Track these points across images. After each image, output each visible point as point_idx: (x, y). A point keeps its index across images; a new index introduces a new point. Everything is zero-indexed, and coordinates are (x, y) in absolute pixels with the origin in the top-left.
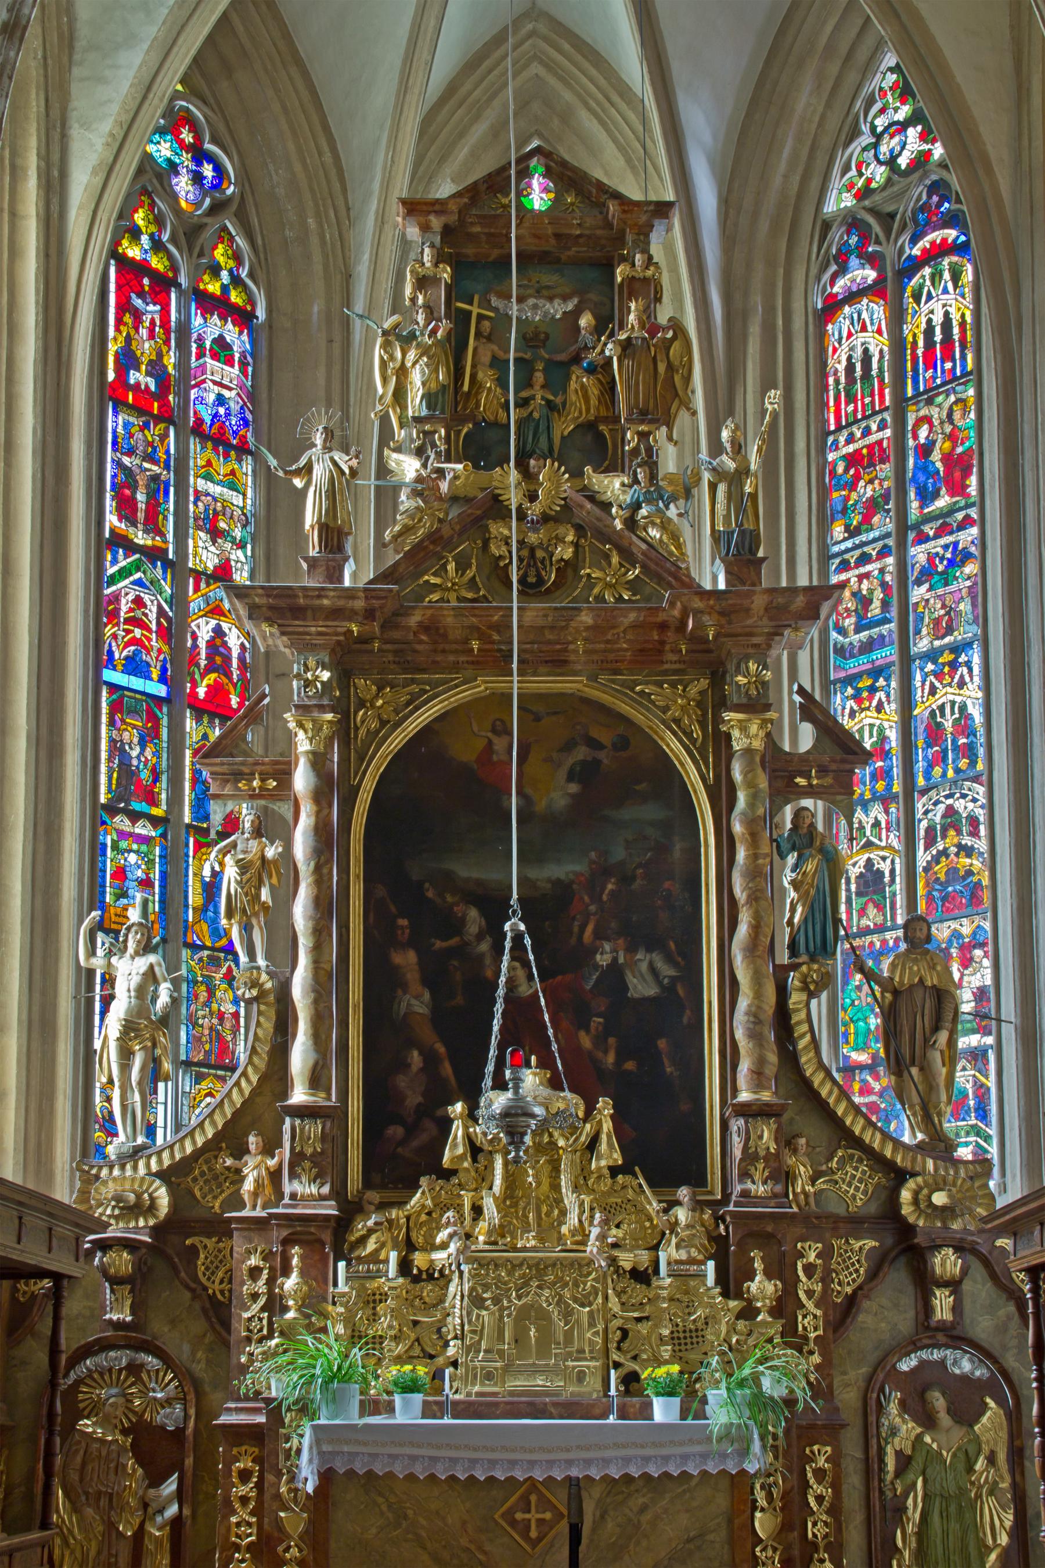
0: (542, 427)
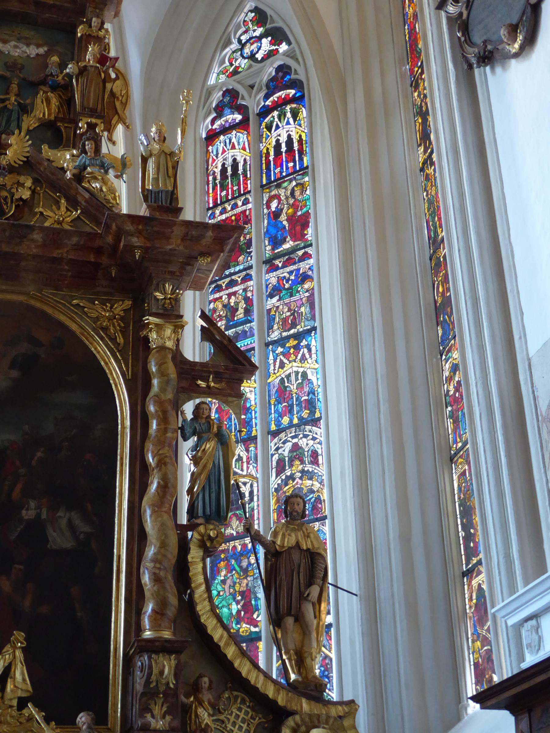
0: (14, 116)
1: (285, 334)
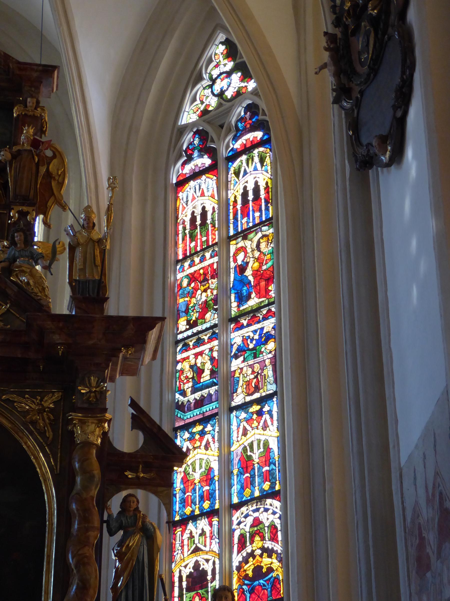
1: (248, 399)
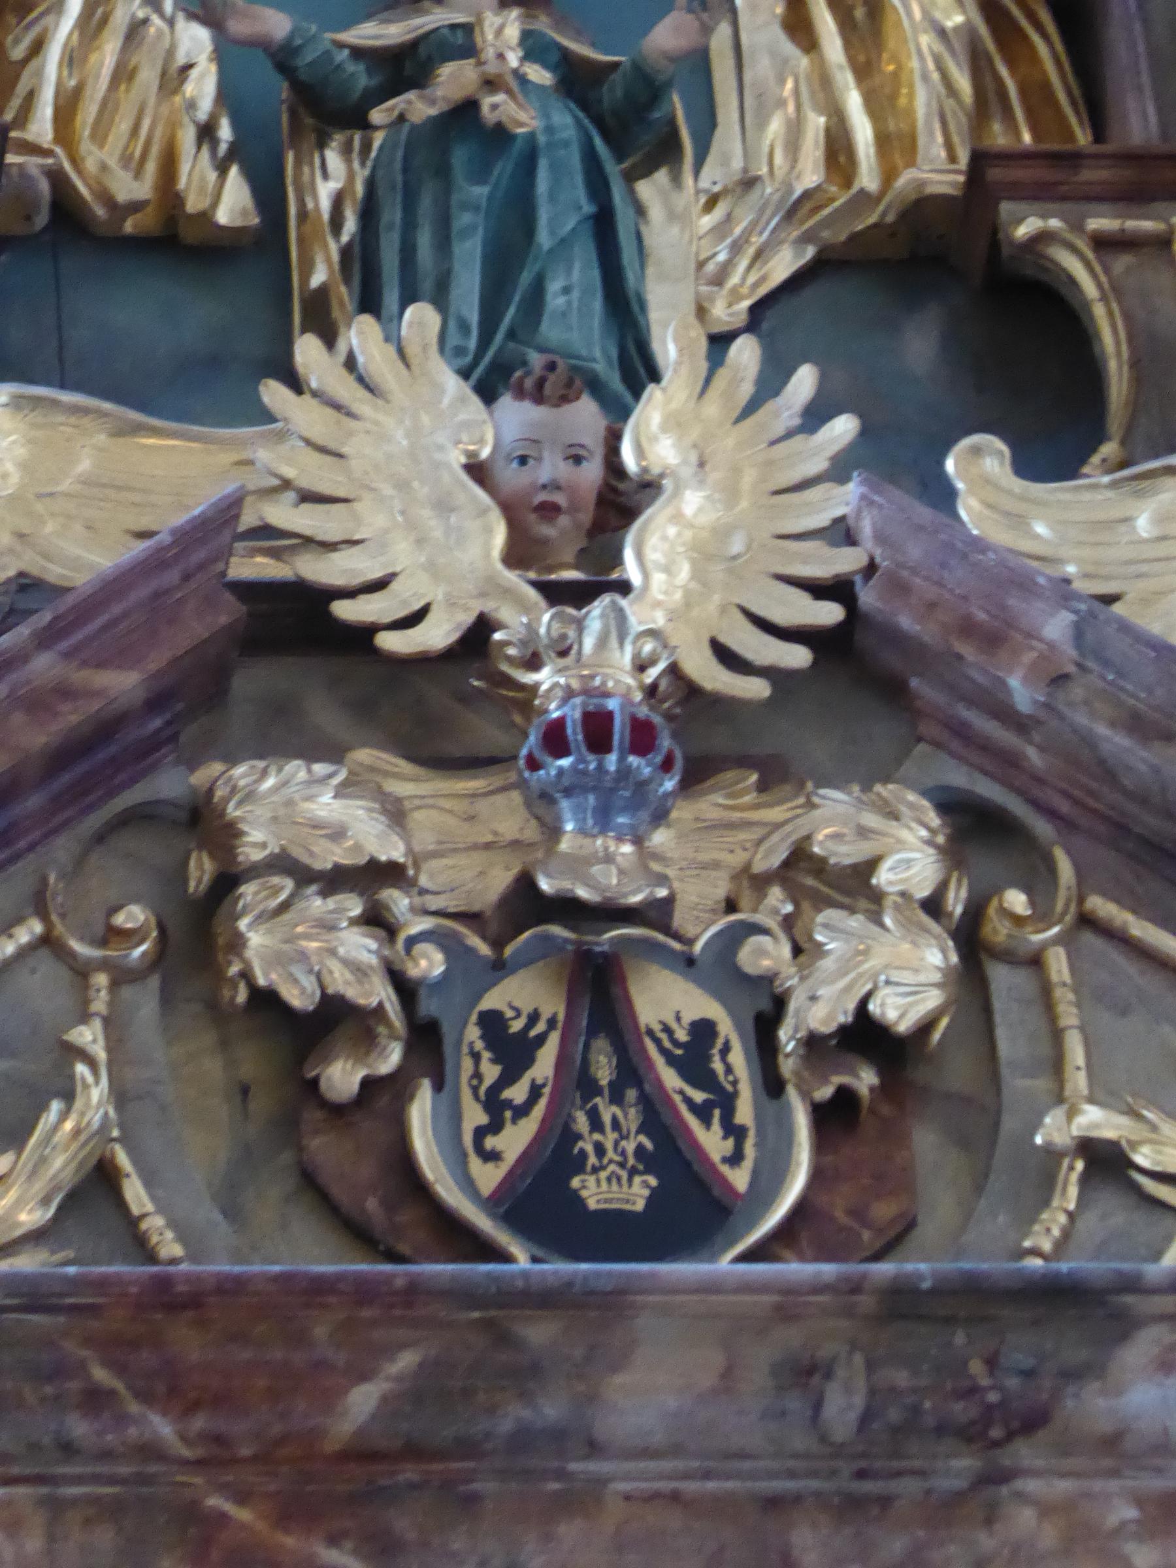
0: (560, 209)
